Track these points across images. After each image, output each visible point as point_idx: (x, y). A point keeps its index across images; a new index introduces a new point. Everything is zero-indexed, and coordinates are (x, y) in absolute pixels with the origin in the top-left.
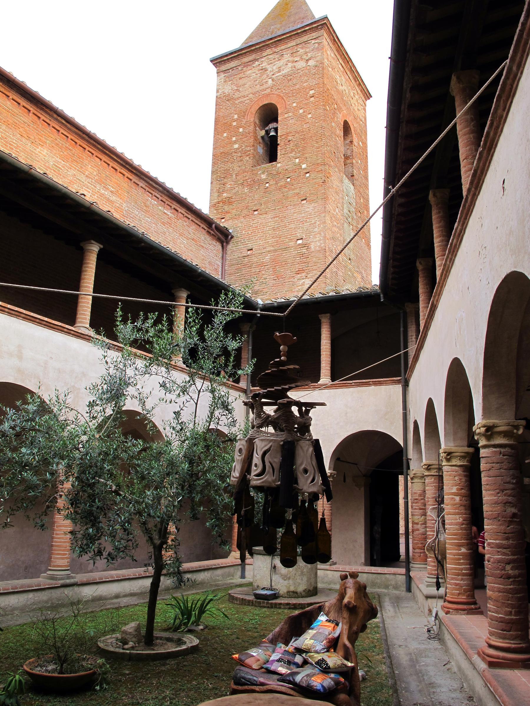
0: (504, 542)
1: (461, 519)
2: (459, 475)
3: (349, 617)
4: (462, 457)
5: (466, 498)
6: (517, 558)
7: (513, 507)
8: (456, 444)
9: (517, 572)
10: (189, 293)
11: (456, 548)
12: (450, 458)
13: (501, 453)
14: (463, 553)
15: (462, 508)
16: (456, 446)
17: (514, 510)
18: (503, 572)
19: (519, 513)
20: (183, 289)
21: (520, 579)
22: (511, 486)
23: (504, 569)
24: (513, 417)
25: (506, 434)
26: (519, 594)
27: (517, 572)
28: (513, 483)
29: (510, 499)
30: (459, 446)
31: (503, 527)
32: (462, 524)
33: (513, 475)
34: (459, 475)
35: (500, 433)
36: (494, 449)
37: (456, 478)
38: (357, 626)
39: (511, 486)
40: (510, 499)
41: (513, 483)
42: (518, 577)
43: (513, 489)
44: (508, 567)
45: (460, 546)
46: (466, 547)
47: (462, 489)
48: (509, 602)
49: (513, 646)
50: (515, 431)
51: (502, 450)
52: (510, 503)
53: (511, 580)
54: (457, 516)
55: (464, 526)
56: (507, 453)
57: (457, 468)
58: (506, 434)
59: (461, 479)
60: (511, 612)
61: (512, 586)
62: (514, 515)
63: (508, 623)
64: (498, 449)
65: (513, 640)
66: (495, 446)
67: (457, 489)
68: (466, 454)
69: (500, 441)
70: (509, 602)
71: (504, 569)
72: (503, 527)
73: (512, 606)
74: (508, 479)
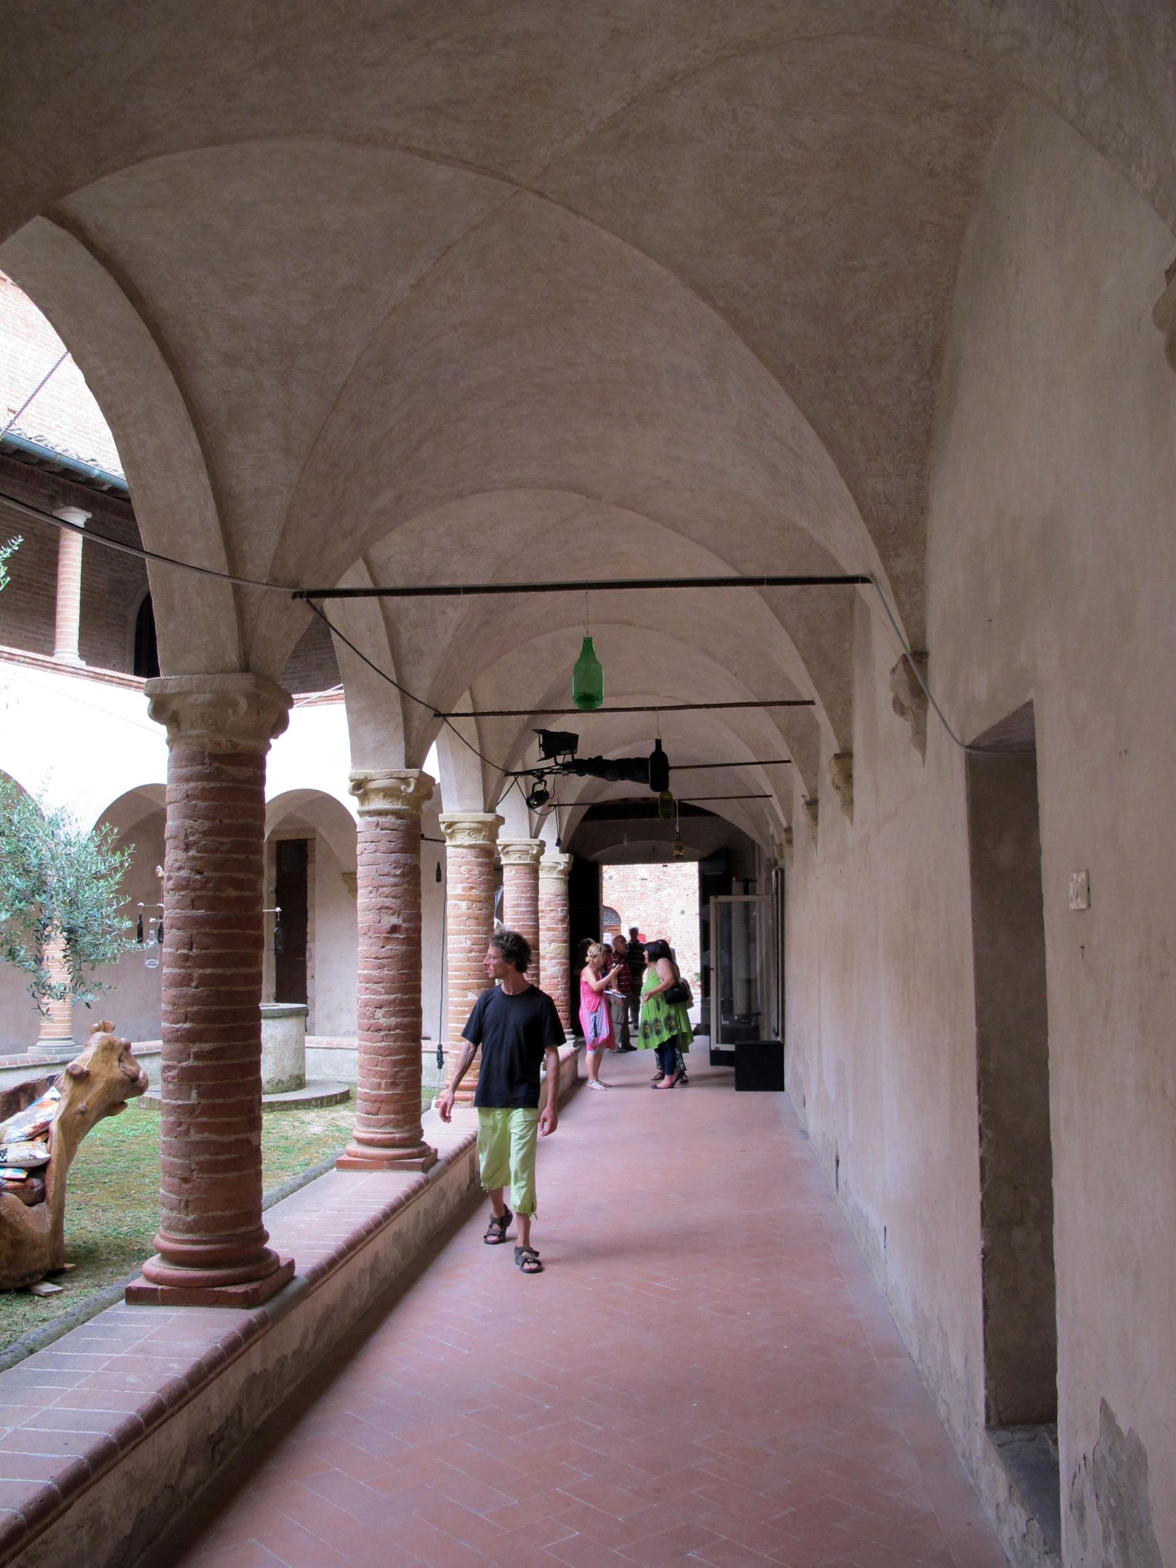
0: (375, 973)
1: (469, 943)
2: (468, 863)
3: (73, 1088)
4: (474, 831)
5: (479, 905)
6: (395, 999)
7: (393, 914)
8: (464, 808)
9: (393, 1021)
10: (90, 515)
11: (460, 992)
12: (453, 832)
13: (377, 825)
14: (471, 1001)
15: (472, 921)
16: (464, 811)
17: (395, 920)
18: (372, 1021)
19: (404, 925)
20: (73, 509)
21: (397, 1031)
22: (392, 880)
23: (372, 1017)
24: (402, 763)
25: (387, 793)
26: (396, 1055)
27: (393, 1021)
28: (395, 876)
29: (389, 902)
30: (470, 811)
31: (374, 949)
32: (471, 951)
33: (396, 862)
34: (468, 863)
35: (377, 791)
36: (370, 819)
37: (463, 869)
38: (88, 1103)
39: (392, 880)
40: (389, 902)
41: (395, 876)
42: (396, 1028)
43: (395, 885)
44: (379, 1013)
45: (466, 988)
46: (477, 991)
47: (472, 888)
48: (378, 1068)
49: (379, 1136)
50: (403, 787)
51: (381, 820)
52: (387, 908)
53: (383, 1033)
54: (463, 937)
55: (473, 954)
56: (387, 825)
57: (464, 850)
58: (387, 793)
59: (470, 871)
60: (380, 1084)
61: (383, 1044)
62: (394, 929)
63: (382, 1102)
64: (374, 819)
65: (380, 1127)
66: (379, 813)
67: (464, 889)
68: (480, 826)
69: (379, 804)
70: (378, 1068)
71: (372, 1017)
72: (374, 949)
73: (382, 1075)
74: (387, 869)
